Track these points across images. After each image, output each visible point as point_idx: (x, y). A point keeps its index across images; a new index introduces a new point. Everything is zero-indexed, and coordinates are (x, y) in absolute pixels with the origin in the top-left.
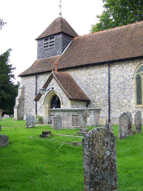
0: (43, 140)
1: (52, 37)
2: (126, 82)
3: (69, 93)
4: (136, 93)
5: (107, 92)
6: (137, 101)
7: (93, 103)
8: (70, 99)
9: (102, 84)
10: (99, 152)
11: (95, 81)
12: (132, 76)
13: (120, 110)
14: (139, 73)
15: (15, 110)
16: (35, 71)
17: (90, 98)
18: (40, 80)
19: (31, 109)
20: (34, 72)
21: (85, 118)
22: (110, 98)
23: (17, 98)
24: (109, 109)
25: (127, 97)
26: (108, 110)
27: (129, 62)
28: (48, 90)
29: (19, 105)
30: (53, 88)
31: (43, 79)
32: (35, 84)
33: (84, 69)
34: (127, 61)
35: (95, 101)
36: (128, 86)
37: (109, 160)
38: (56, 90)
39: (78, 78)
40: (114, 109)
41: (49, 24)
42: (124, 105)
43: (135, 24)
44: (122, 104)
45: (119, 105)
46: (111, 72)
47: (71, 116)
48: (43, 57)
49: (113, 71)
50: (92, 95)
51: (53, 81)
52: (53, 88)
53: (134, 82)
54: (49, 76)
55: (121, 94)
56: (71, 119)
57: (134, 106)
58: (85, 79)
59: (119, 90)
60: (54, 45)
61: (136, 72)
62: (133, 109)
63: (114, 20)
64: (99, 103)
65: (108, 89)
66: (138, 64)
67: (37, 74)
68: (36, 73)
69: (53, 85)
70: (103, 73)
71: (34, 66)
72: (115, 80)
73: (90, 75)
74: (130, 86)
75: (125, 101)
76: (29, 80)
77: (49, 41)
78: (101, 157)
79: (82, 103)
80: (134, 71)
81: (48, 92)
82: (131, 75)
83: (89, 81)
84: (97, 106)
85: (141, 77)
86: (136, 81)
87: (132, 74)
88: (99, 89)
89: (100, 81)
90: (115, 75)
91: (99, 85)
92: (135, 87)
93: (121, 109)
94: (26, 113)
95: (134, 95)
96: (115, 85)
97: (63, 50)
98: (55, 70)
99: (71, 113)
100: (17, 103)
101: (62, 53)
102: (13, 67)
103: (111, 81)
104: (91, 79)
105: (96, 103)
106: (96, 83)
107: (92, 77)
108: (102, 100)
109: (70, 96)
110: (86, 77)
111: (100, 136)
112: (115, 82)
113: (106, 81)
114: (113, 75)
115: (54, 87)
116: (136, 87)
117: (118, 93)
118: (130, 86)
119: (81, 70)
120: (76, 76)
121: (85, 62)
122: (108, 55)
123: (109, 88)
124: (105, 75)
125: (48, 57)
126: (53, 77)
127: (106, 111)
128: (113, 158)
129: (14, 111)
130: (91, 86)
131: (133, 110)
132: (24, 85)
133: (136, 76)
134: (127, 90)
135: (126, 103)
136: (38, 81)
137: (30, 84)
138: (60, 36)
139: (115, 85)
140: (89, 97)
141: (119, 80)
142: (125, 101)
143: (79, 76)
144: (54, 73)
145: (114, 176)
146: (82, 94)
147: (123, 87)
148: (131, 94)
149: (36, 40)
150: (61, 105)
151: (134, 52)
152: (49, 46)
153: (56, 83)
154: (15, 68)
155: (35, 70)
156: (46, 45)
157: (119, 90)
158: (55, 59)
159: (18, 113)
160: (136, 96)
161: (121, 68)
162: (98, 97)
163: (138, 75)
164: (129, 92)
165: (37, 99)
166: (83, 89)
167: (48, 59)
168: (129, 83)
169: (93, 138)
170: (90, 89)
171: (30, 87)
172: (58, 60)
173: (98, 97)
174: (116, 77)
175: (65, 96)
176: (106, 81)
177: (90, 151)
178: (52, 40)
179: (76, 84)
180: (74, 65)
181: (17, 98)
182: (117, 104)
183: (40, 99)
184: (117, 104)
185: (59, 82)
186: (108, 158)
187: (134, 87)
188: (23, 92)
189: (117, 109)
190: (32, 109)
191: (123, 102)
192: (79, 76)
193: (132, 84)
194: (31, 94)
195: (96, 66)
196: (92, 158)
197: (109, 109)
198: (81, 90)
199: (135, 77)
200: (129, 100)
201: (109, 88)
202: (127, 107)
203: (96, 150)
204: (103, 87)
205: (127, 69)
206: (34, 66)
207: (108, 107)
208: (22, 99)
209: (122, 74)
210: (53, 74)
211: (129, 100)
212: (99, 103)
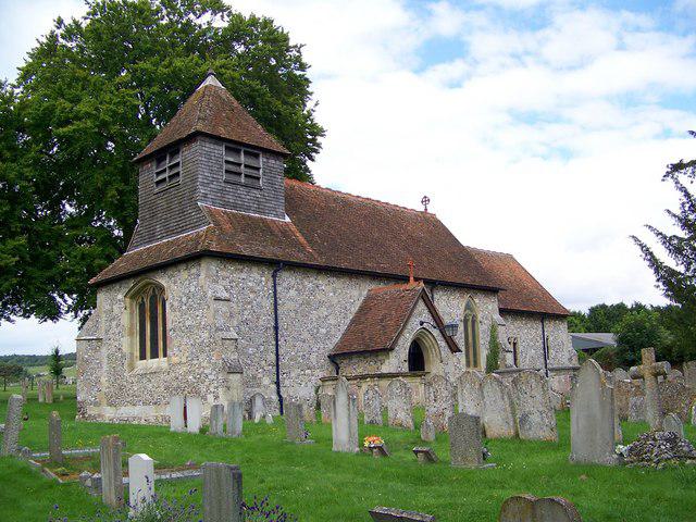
76: (243, 275)
137: (247, 291)
190: (260, 375)
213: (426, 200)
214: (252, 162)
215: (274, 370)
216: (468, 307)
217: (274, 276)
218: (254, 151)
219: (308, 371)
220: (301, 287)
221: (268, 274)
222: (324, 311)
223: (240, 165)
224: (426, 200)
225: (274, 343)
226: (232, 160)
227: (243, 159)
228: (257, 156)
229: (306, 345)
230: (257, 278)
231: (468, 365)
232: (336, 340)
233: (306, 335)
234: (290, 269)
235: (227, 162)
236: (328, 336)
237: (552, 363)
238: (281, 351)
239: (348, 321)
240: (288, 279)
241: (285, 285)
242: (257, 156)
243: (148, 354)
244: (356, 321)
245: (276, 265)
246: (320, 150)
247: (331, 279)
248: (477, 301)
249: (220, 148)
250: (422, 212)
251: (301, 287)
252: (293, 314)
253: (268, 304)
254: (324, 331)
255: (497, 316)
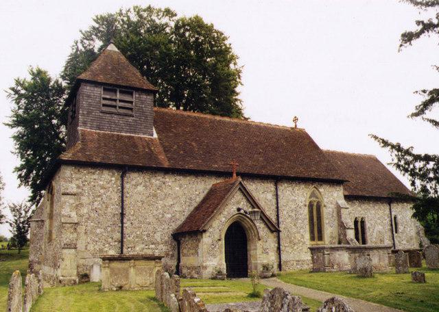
0: (317, 277)
18: (134, 182)
21: (99, 290)
33: (357, 203)
41: (64, 64)
42: (297, 241)
45: (290, 242)
63: (435, 216)
69: (238, 203)
76: (95, 176)
95: (308, 228)
119: (209, 179)
136: (127, 186)
137: (98, 188)
139: (285, 212)
142: (298, 236)
161: (290, 189)
190: (106, 249)
202: (301, 245)
213: (296, 120)
214: (127, 98)
215: (120, 245)
216: (313, 195)
217: (122, 177)
218: (128, 90)
219: (153, 246)
220: (148, 184)
221: (117, 175)
222: (170, 202)
223: (115, 100)
224: (296, 120)
225: (120, 225)
226: (108, 97)
227: (118, 96)
228: (131, 94)
229: (150, 228)
230: (107, 179)
231: (312, 238)
232: (179, 223)
233: (150, 219)
234: (203, 176)
235: (104, 99)
236: (173, 219)
237: (388, 243)
238: (125, 231)
239: (192, 208)
240: (134, 178)
241: (134, 182)
242: (131, 94)
243: (316, 239)
244: (197, 209)
245: (124, 169)
246: (13, 85)
247: (178, 178)
248: (321, 190)
249: (99, 90)
250: (292, 128)
251: (148, 184)
252: (140, 204)
253: (116, 197)
254: (169, 216)
255: (342, 202)
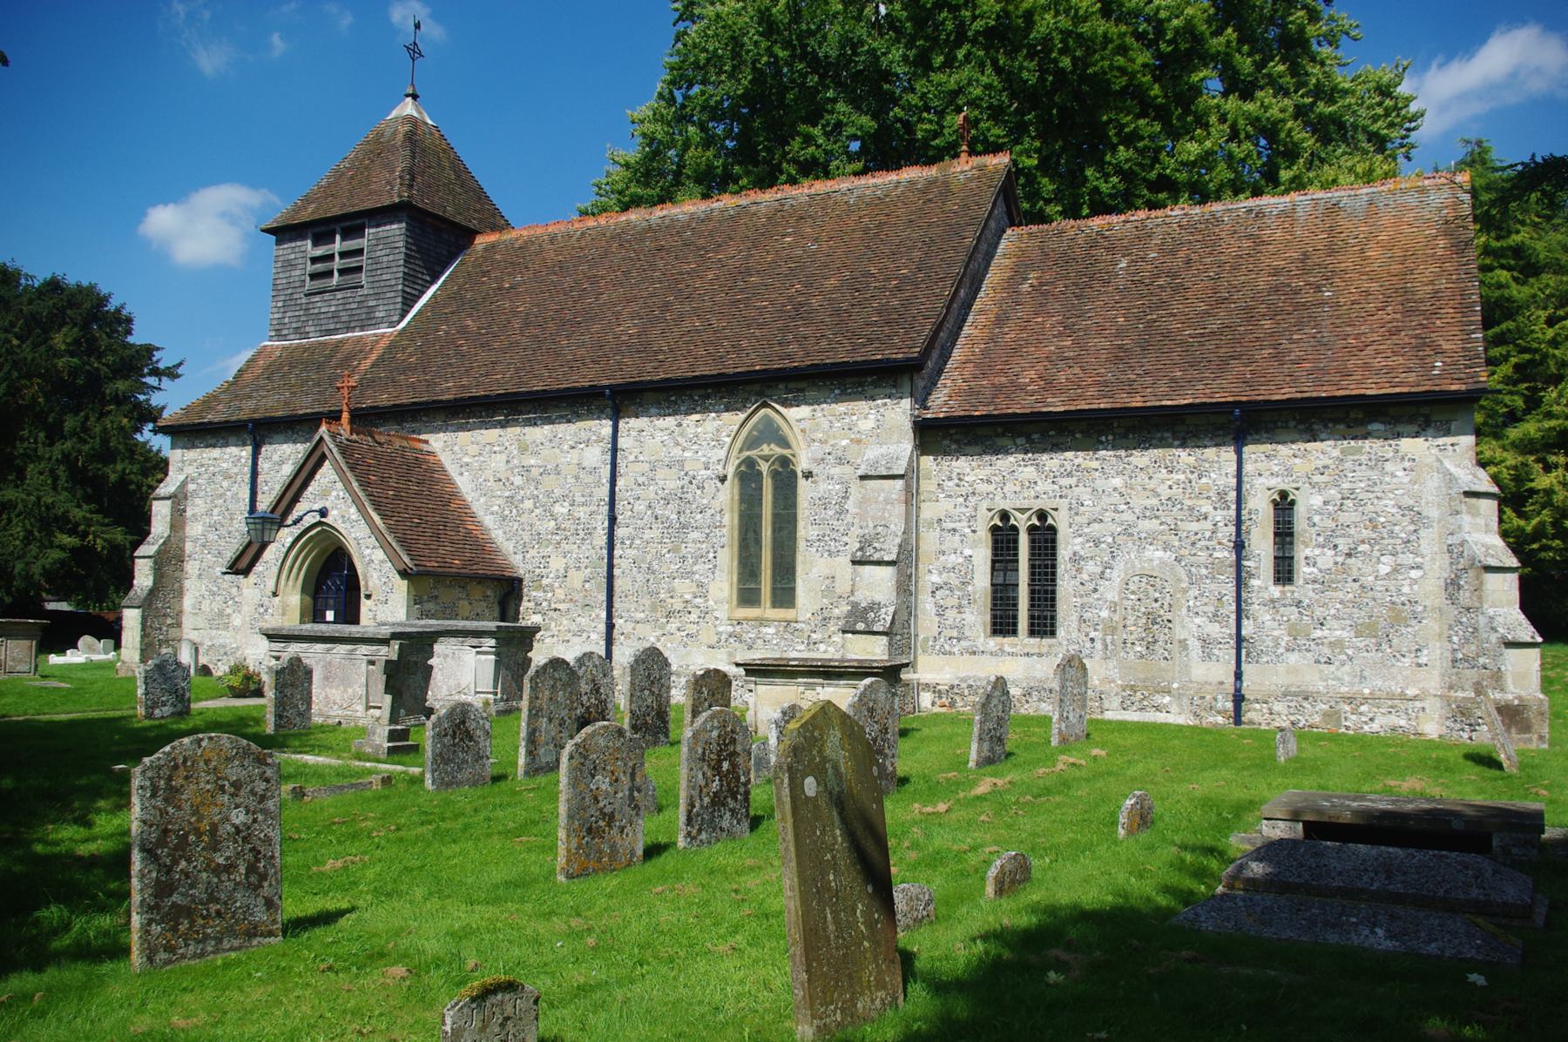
1: (352, 224)
2: (689, 496)
3: (401, 541)
4: (736, 549)
5: (601, 539)
6: (740, 590)
7: (534, 593)
8: (404, 574)
9: (579, 499)
10: (195, 812)
11: (549, 482)
12: (720, 468)
13: (659, 633)
14: (753, 453)
15: (131, 619)
16: (247, 409)
17: (520, 564)
19: (221, 614)
20: (243, 416)
22: (616, 572)
23: (148, 549)
24: (610, 627)
25: (695, 568)
26: (602, 627)
27: (708, 397)
28: (295, 523)
29: (153, 592)
30: (323, 513)
31: (282, 458)
32: (247, 478)
34: (702, 392)
35: (545, 582)
36: (699, 516)
37: (244, 839)
38: (340, 526)
39: (466, 459)
40: (630, 626)
42: (678, 605)
43: (779, 196)
44: (670, 600)
45: (654, 608)
46: (623, 442)
47: (364, 665)
48: (301, 332)
49: (633, 433)
50: (533, 552)
51: (326, 473)
52: (323, 513)
53: (726, 497)
54: (308, 446)
55: (665, 551)
56: (363, 680)
57: (722, 612)
58: (502, 466)
59: (655, 533)
60: (359, 269)
61: (739, 444)
62: (721, 629)
64: (560, 594)
65: (606, 524)
66: (742, 416)
67: (258, 431)
68: (250, 420)
69: (324, 494)
70: (588, 442)
71: (248, 376)
72: (641, 480)
73: (523, 449)
74: (710, 512)
75: (684, 588)
77: (338, 245)
78: (205, 826)
79: (477, 591)
80: (728, 440)
81: (297, 530)
82: (714, 459)
83: (518, 481)
84: (553, 606)
85: (760, 473)
86: (736, 491)
87: (722, 454)
88: (567, 524)
89: (571, 480)
90: (641, 458)
91: (566, 504)
92: (730, 520)
93: (662, 628)
94: (194, 636)
95: (727, 559)
96: (640, 507)
97: (409, 302)
98: (338, 418)
99: (364, 649)
100: (143, 577)
101: (403, 317)
102: (164, 360)
103: (620, 483)
104: (527, 469)
105: (550, 595)
106: (549, 494)
107: (532, 462)
108: (576, 578)
109: (406, 559)
110: (504, 457)
111: (207, 762)
112: (638, 491)
113: (599, 484)
114: (632, 458)
115: (328, 504)
116: (736, 521)
117: (652, 550)
118: (710, 512)
120: (456, 448)
121: (502, 382)
122: (619, 352)
123: (613, 520)
124: (596, 456)
125: (329, 332)
126: (323, 458)
127: (594, 636)
128: (262, 835)
129: (124, 623)
130: (528, 504)
131: (721, 633)
132: (184, 484)
133: (739, 465)
134: (695, 535)
135: (688, 597)
138: (395, 231)
139: (640, 507)
140: (516, 560)
141: (661, 483)
143: (473, 449)
144: (334, 436)
145: (266, 890)
146: (480, 546)
147: (674, 516)
148: (711, 555)
149: (263, 231)
150: (365, 605)
151: (737, 348)
152: (336, 274)
153: (340, 485)
154: (172, 373)
155: (251, 404)
156: (320, 267)
157: (655, 533)
158: (360, 349)
159: (144, 635)
160: (736, 563)
162: (557, 564)
163: (750, 463)
164: (704, 546)
165: (242, 565)
166: (488, 521)
167: (325, 344)
168: (705, 501)
169: (176, 767)
170: (524, 519)
171: (221, 491)
172: (374, 357)
173: (557, 564)
174: (646, 467)
175: (380, 554)
176: (599, 484)
177: (160, 810)
178: (352, 244)
179: (455, 495)
180: (448, 390)
181: (143, 550)
182: (647, 601)
183: (259, 568)
184: (647, 601)
185: (355, 485)
186: (238, 831)
187: (726, 520)
188: (178, 520)
189: (648, 627)
190: (229, 611)
191: (672, 593)
192: (473, 449)
193: (716, 505)
194: (223, 531)
195: (557, 406)
196: (166, 831)
197: (610, 627)
198: (480, 524)
199: (730, 471)
200: (700, 585)
201: (613, 520)
202: (693, 617)
203: (187, 806)
204: (582, 513)
205: (699, 430)
206: (248, 376)
207: (604, 615)
208: (170, 561)
209: (677, 451)
210: (326, 438)
211: (700, 585)
212: (560, 594)
